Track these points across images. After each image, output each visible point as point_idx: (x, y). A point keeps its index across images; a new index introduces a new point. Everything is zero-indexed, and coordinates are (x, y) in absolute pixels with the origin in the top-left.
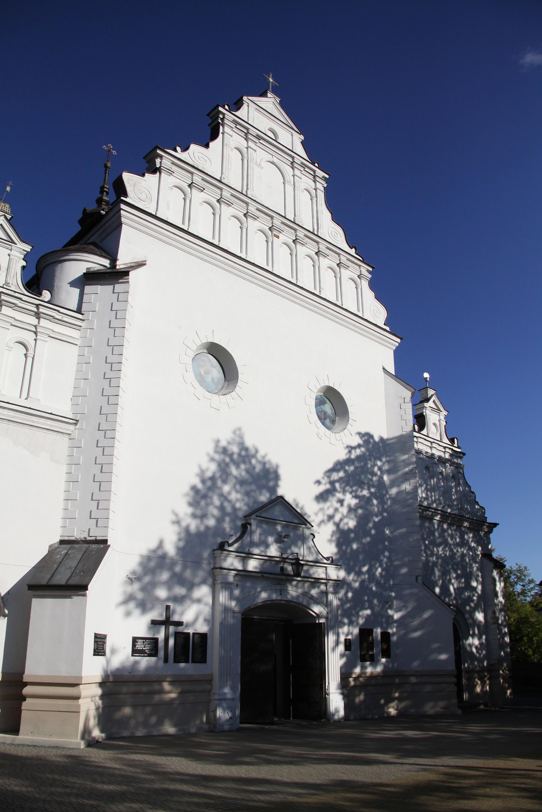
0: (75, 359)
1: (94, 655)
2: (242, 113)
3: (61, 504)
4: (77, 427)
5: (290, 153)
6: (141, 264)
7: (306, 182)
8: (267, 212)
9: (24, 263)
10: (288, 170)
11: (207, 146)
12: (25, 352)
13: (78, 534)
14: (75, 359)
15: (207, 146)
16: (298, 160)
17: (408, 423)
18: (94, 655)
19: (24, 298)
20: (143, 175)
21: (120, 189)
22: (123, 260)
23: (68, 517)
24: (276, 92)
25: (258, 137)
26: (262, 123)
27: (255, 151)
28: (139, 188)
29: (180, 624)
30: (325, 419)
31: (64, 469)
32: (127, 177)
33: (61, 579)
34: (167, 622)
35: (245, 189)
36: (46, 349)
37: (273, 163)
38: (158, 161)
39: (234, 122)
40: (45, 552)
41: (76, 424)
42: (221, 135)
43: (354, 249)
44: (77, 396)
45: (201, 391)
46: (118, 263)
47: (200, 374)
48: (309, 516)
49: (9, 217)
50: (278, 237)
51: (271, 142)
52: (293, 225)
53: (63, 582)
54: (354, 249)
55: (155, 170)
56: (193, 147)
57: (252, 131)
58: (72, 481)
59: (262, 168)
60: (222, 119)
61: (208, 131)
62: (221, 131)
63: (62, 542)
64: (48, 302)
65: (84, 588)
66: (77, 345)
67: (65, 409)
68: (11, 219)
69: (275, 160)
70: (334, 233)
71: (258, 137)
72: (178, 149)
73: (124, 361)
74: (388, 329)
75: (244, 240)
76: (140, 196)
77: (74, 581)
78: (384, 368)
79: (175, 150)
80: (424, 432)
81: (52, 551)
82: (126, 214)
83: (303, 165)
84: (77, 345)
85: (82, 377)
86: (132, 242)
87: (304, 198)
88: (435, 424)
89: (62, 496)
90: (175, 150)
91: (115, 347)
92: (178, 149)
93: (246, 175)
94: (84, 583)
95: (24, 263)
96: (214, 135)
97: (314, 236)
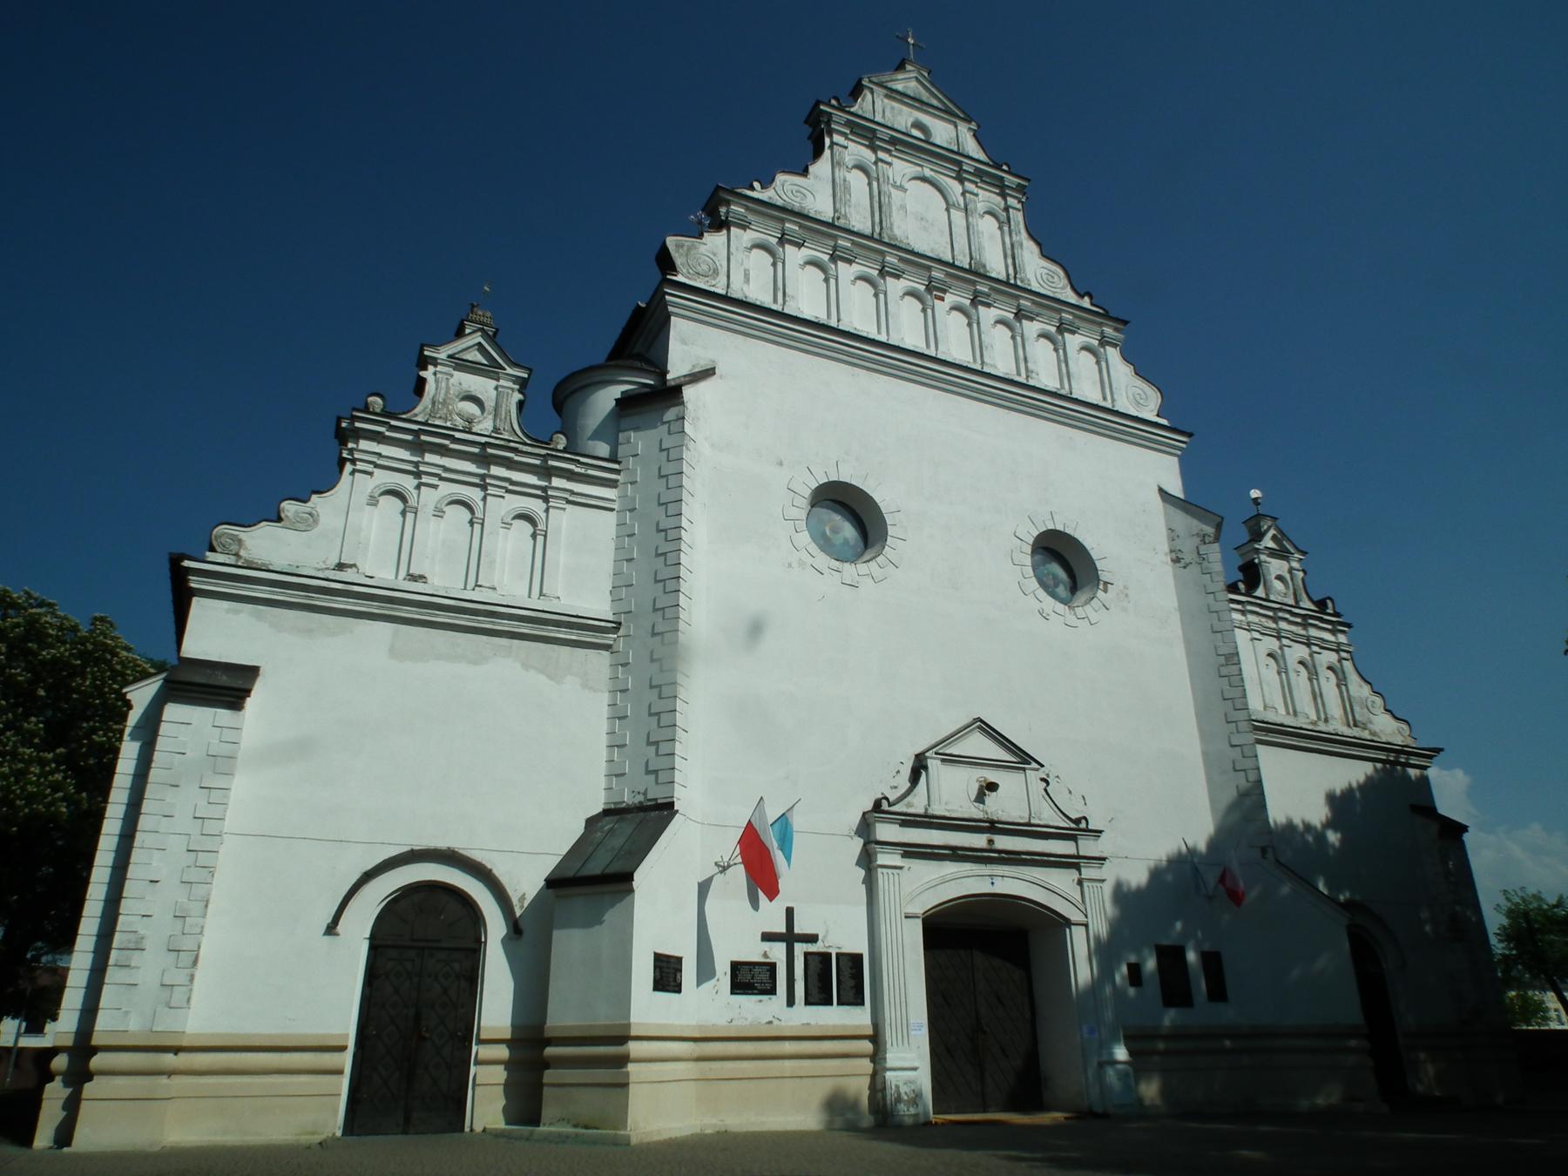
0: (613, 531)
1: (679, 991)
2: (864, 105)
3: (604, 754)
4: (621, 632)
5: (952, 159)
6: (708, 373)
7: (986, 198)
8: (915, 260)
9: (520, 397)
10: (955, 187)
11: (804, 172)
12: (469, 516)
13: (628, 798)
14: (612, 531)
15: (804, 172)
16: (968, 166)
17: (1216, 578)
18: (679, 991)
19: (525, 448)
20: (701, 236)
21: (666, 262)
22: (677, 368)
23: (616, 774)
24: (921, 63)
25: (893, 141)
26: (902, 117)
27: (890, 164)
28: (730, 259)
29: (812, 939)
30: (1056, 585)
31: (605, 698)
32: (671, 242)
33: (595, 868)
34: (790, 937)
35: (877, 230)
36: (564, 521)
37: (924, 179)
38: (723, 210)
39: (848, 123)
40: (578, 829)
41: (618, 629)
42: (827, 152)
43: (1087, 299)
44: (620, 586)
45: (823, 560)
46: (669, 377)
47: (824, 534)
48: (393, 652)
49: (491, 331)
50: (942, 299)
51: (916, 147)
52: (976, 273)
53: (598, 871)
54: (1087, 299)
55: (720, 225)
56: (780, 178)
57: (884, 133)
58: (618, 716)
59: (905, 190)
60: (828, 123)
61: (810, 147)
62: (827, 141)
63: (606, 812)
64: (565, 450)
65: (629, 877)
66: (612, 510)
67: (596, 604)
68: (495, 334)
69: (928, 173)
70: (1038, 271)
71: (893, 141)
72: (756, 185)
73: (685, 523)
74: (1164, 422)
75: (883, 314)
76: (699, 269)
77: (616, 867)
78: (1161, 490)
79: (752, 188)
80: (1260, 592)
81: (591, 822)
82: (672, 298)
83: (979, 173)
84: (612, 510)
85: (624, 558)
86: (688, 343)
87: (987, 227)
88: (1279, 578)
89: (604, 740)
90: (752, 188)
91: (671, 505)
92: (756, 185)
93: (879, 206)
94: (628, 869)
95: (520, 397)
96: (818, 152)
97: (1010, 288)
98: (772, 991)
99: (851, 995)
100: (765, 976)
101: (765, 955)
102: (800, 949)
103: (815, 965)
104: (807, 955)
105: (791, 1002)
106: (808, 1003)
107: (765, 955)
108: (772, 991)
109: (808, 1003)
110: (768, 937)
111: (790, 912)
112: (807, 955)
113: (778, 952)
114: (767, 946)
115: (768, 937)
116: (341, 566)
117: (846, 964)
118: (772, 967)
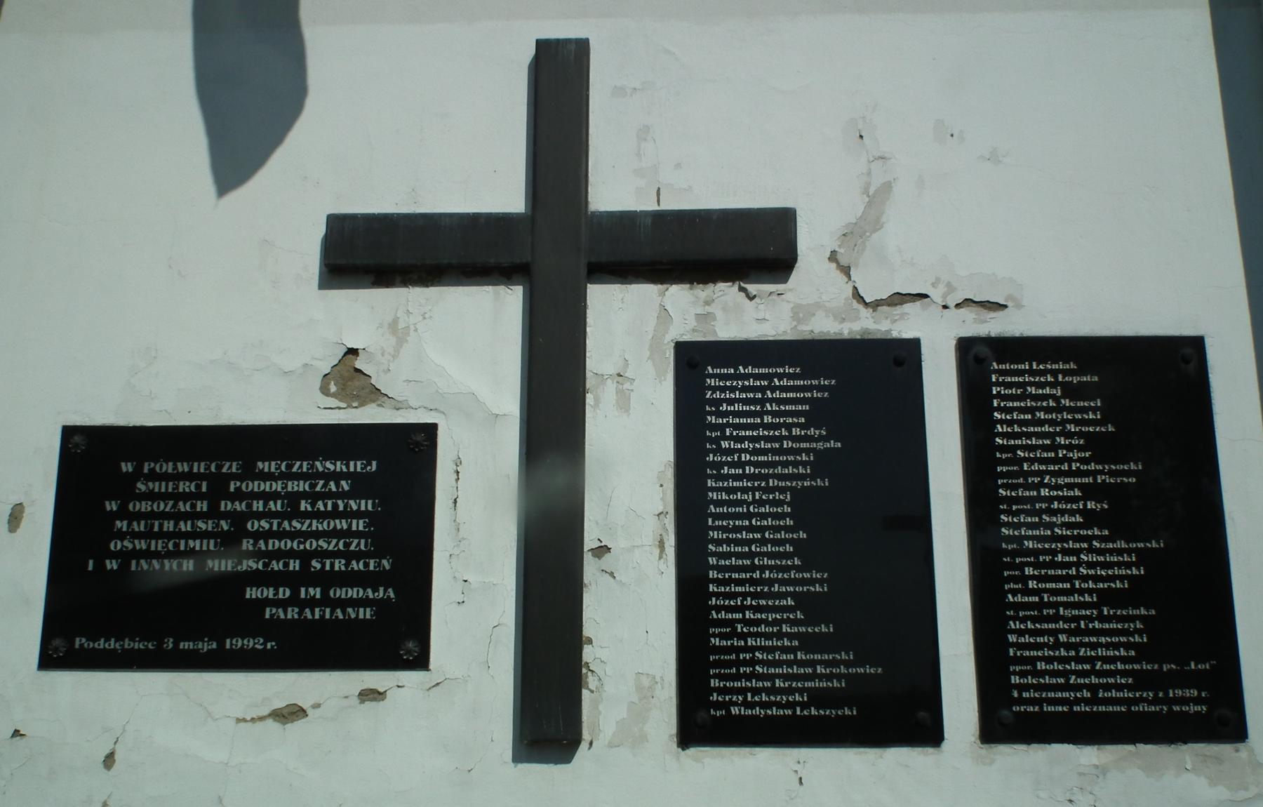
29: (751, 247)
34: (551, 249)
98: (393, 635)
99: (782, 663)
100: (339, 527)
101: (348, 375)
102: (633, 331)
103: (775, 439)
104: (693, 361)
105: (549, 715)
106: (707, 717)
107: (348, 375)
108: (393, 635)
109: (707, 717)
110: (369, 252)
111: (559, 80)
112: (693, 361)
113: (453, 360)
114: (364, 314)
115: (369, 252)
116: (291, 714)
117: (1053, 427)
118: (401, 462)
